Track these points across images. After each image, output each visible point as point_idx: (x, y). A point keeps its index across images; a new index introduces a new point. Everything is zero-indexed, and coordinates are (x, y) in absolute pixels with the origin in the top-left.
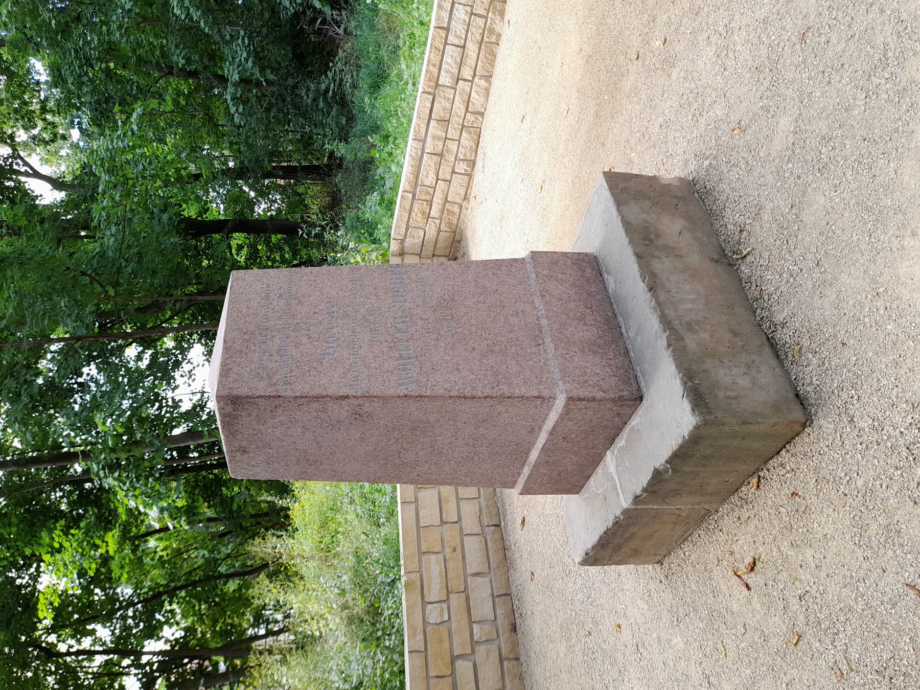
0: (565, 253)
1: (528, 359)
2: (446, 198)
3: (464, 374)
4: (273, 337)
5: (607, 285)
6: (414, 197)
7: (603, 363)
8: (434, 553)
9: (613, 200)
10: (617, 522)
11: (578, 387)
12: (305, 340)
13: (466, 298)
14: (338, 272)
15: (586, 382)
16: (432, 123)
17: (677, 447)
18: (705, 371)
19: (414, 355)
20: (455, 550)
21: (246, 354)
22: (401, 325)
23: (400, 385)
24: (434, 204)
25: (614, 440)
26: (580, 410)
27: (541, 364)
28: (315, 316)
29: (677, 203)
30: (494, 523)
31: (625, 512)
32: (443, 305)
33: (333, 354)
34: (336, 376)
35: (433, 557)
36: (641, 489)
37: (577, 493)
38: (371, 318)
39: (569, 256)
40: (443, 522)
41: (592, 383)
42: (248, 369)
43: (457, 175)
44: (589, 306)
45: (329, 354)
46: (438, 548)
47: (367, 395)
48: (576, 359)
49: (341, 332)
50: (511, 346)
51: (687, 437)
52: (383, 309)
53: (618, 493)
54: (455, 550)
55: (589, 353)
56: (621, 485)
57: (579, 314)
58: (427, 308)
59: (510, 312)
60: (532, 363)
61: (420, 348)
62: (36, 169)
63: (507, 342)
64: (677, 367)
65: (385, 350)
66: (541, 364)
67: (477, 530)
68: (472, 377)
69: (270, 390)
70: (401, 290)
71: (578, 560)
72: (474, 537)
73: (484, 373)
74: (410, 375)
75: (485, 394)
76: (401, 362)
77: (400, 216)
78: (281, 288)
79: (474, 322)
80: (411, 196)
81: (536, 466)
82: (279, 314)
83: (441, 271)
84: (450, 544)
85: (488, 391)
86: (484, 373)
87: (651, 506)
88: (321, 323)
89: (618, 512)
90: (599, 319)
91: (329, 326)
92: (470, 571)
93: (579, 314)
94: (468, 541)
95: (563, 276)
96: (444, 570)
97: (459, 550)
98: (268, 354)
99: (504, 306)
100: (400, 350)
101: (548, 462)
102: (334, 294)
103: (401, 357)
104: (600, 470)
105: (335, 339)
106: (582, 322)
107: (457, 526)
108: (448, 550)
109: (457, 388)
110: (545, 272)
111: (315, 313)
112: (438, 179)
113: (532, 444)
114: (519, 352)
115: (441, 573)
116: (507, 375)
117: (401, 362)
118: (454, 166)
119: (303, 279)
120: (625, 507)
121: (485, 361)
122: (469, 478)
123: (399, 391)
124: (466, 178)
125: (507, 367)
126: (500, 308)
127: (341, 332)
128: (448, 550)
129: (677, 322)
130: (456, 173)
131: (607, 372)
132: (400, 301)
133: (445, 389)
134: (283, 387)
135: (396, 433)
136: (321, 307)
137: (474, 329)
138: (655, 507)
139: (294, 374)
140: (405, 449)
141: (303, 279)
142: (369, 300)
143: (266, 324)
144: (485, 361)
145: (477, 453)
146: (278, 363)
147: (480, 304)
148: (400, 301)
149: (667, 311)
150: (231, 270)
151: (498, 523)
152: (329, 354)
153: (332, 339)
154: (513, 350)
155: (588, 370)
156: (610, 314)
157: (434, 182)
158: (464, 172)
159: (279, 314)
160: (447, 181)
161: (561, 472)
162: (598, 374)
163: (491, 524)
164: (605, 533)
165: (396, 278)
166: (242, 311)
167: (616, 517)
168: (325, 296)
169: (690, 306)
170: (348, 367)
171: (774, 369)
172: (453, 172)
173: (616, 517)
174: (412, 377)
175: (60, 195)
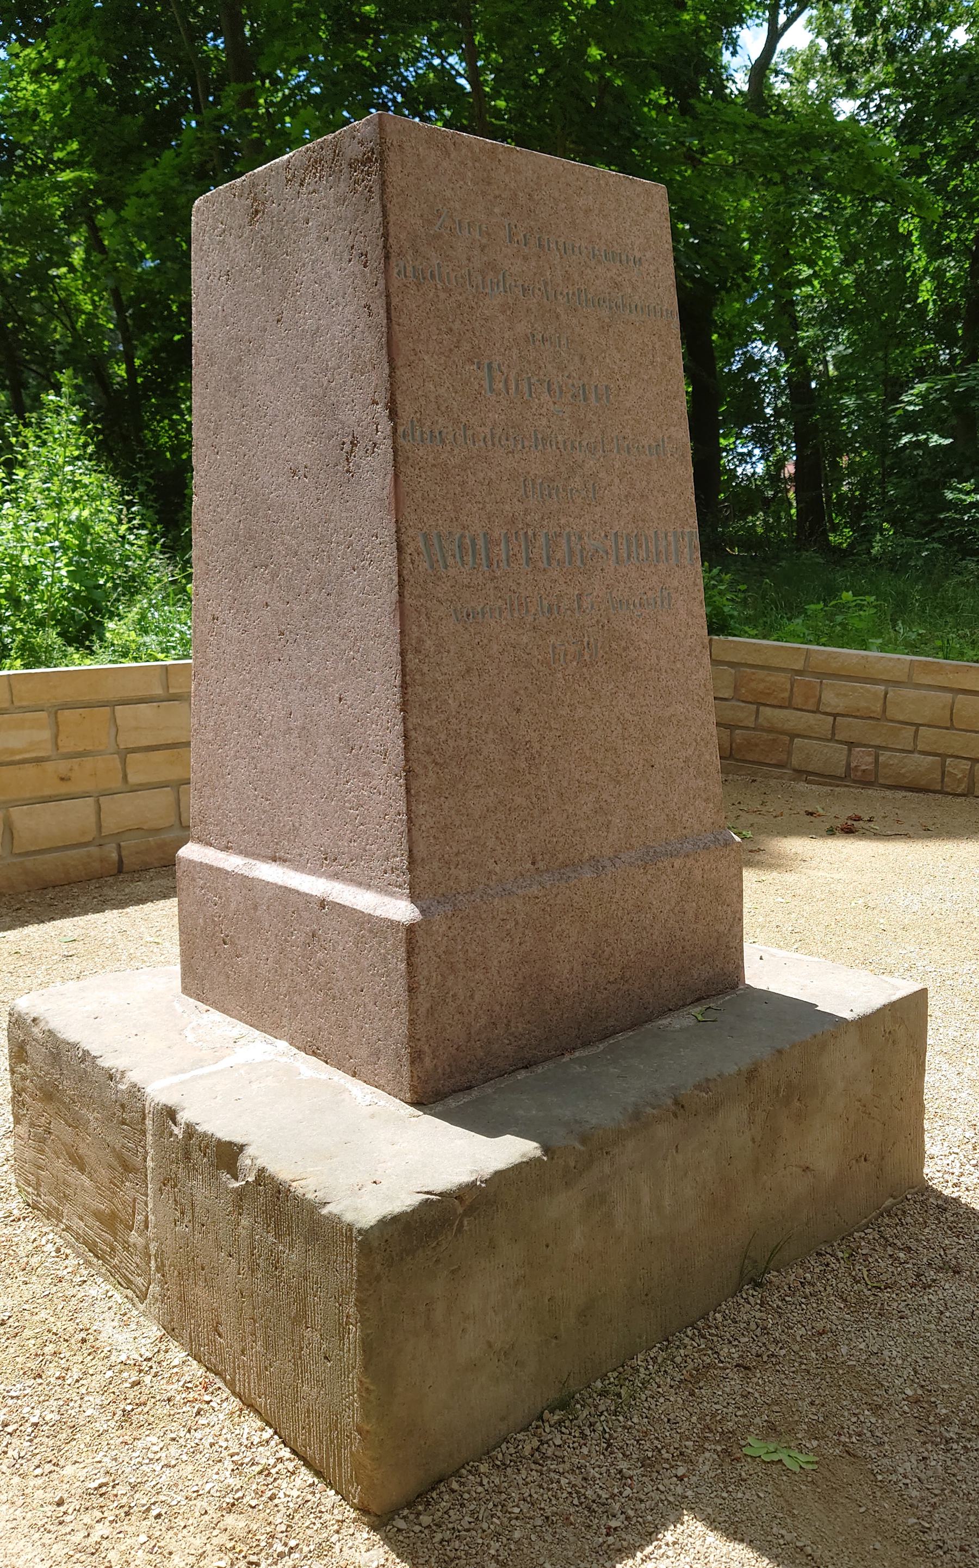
0: (741, 919)
1: (501, 834)
2: (799, 736)
3: (458, 687)
4: (525, 258)
5: (676, 1014)
6: (798, 672)
7: (497, 1008)
8: (56, 736)
9: (869, 1011)
10: (111, 1078)
11: (440, 951)
12: (521, 328)
13: (632, 696)
14: (675, 416)
15: (452, 968)
16: (949, 696)
17: (300, 1191)
18: (493, 1246)
19: (498, 573)
20: (62, 779)
21: (484, 194)
22: (565, 547)
23: (426, 537)
24: (786, 712)
25: (314, 1054)
26: (385, 959)
27: (491, 865)
28: (576, 358)
29: (871, 1159)
30: (125, 861)
31: (136, 1091)
32: (614, 645)
33: (492, 390)
34: (442, 391)
35: (46, 734)
36: (193, 1120)
37: (186, 990)
38: (577, 482)
39: (736, 929)
40: (124, 754)
41: (449, 984)
42: (448, 193)
43: (846, 752)
44: (628, 974)
45: (492, 379)
46: (67, 745)
47: (400, 459)
48: (506, 945)
49: (544, 411)
50: (528, 797)
51: (324, 1211)
52: (598, 509)
53: (183, 1071)
54: (62, 779)
55: (520, 976)
56: (201, 1077)
57: (608, 950)
58: (607, 609)
59: (605, 796)
60: (490, 844)
61: (514, 587)
62: (786, 34)
63: (538, 788)
64: (498, 1174)
65: (507, 507)
66: (491, 865)
67: (110, 825)
68: (453, 704)
69: (403, 236)
70: (643, 554)
71: (25, 1004)
72: (93, 819)
73: (464, 732)
74: (450, 561)
75: (413, 733)
76: (481, 542)
77: (758, 649)
78: (634, 288)
79: (580, 712)
80: (798, 666)
81: (247, 883)
82: (576, 276)
83: (688, 643)
84: (76, 767)
85: (421, 740)
86: (464, 732)
87: (151, 1152)
88: (562, 368)
89: (134, 1076)
90: (599, 996)
91: (555, 387)
92: (15, 812)
93: (608, 950)
94: (85, 807)
95: (691, 914)
96: (18, 757)
97: (64, 789)
98: (484, 241)
99: (618, 782)
100: (507, 542)
101: (255, 908)
102: (628, 405)
103: (489, 540)
104: (241, 1028)
105: (526, 396)
106: (590, 959)
107: (117, 784)
108: (62, 766)
109: (425, 669)
110: (698, 873)
111: (583, 358)
112: (835, 716)
113: (300, 866)
114: (514, 815)
115: (13, 752)
116: (460, 786)
117: (481, 542)
118: (865, 746)
119: (655, 339)
120: (148, 1090)
121: (491, 735)
122: (210, 736)
123: (411, 532)
124: (841, 772)
125: (478, 787)
126: (613, 773)
127: (544, 411)
128: (62, 766)
129: (607, 1170)
130: (850, 750)
131: (477, 1017)
132: (617, 549)
133: (420, 640)
134: (410, 269)
135: (310, 546)
136: (596, 372)
137: (564, 711)
138: (150, 1164)
139: (443, 295)
140: (274, 575)
141: (655, 339)
142: (617, 481)
143: (553, 246)
144: (491, 735)
145: (271, 741)
146: (465, 262)
147: (619, 728)
148: (617, 549)
149: (630, 1144)
150: (669, 184)
151: (124, 870)
152: (492, 379)
153: (526, 389)
154: (519, 800)
155: (479, 976)
156: (611, 1022)
157: (828, 710)
158: (853, 765)
159: (576, 276)
160: (833, 734)
161: (232, 943)
162: (472, 997)
163: (123, 853)
164: (86, 1053)
165: (669, 544)
166: (579, 195)
167: (123, 1072)
168: (621, 383)
169: (646, 1199)
170: (464, 419)
171: (503, 1419)
172: (851, 745)
173: (123, 1072)
174: (446, 567)
175: (740, 83)
